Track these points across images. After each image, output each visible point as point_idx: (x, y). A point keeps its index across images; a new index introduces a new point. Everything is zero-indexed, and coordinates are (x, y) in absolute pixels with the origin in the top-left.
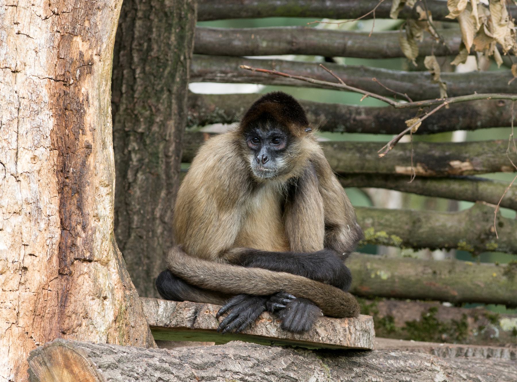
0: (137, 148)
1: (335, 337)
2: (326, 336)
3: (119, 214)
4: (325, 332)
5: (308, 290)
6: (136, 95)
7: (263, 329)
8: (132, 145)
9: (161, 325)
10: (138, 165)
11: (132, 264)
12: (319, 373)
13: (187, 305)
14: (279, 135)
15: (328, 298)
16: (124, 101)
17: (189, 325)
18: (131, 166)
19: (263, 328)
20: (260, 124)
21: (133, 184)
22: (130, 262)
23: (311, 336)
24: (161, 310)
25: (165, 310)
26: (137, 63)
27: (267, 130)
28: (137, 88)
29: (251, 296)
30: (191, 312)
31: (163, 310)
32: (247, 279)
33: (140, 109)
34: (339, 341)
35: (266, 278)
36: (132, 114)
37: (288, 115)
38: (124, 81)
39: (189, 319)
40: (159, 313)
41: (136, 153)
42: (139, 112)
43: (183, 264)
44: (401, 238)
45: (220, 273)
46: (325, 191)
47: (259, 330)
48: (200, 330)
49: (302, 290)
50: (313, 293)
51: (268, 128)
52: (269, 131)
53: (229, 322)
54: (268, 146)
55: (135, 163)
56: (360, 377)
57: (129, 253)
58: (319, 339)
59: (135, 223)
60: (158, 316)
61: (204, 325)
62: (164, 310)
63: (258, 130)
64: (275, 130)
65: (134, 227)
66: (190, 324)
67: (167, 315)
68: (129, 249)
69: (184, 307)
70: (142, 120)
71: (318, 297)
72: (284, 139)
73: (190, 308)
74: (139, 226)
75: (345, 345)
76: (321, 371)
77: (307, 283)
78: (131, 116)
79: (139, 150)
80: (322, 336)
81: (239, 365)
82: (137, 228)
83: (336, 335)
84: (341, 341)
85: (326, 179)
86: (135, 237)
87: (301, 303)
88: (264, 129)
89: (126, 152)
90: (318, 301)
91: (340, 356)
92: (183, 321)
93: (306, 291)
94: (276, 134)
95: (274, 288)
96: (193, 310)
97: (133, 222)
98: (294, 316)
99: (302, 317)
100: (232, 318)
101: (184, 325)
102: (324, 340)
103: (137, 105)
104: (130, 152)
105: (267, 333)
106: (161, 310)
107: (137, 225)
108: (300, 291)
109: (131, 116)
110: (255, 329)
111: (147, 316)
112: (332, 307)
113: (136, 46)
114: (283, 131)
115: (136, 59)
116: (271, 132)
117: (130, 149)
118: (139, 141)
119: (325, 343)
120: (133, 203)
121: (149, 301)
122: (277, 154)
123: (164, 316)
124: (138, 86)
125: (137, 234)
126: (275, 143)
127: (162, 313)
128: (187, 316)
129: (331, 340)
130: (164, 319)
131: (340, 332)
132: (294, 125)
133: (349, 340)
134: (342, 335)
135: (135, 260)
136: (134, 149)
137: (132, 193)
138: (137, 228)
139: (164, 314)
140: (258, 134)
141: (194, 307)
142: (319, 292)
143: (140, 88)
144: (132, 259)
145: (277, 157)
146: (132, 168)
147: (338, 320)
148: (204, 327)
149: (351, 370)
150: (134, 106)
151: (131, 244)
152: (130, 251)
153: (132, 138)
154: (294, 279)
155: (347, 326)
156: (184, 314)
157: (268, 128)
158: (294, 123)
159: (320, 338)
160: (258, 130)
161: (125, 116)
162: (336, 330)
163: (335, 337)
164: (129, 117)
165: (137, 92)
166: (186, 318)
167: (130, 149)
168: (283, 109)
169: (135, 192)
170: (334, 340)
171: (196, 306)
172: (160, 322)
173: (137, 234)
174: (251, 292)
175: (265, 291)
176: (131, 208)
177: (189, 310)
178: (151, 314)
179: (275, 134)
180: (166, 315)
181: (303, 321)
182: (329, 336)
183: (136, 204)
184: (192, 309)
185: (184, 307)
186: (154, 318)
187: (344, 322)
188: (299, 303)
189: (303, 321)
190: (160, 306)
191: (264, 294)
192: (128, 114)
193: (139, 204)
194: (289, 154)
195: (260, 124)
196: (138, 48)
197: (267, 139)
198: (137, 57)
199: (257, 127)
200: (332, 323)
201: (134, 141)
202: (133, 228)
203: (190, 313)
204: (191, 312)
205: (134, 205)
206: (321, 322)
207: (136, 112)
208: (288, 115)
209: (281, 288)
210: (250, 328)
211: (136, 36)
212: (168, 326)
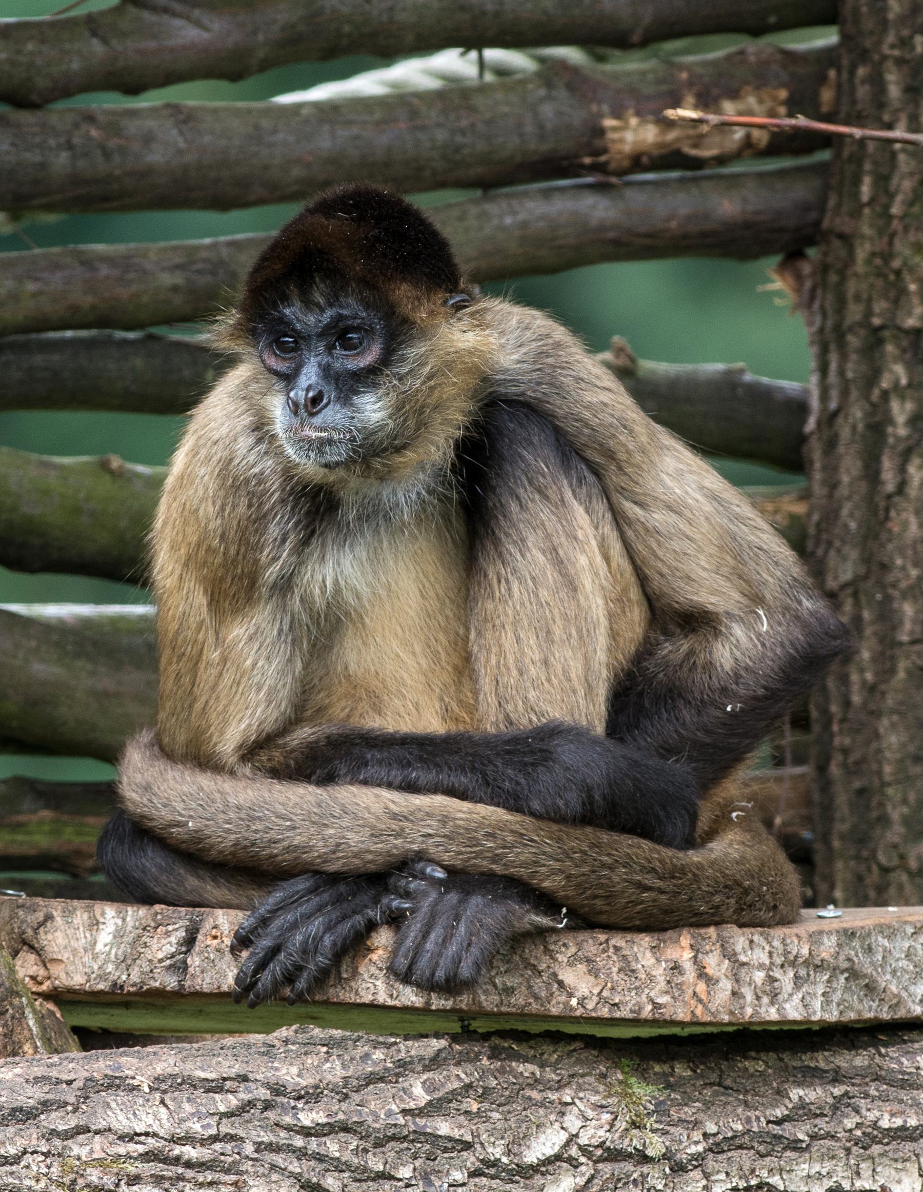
0: (904, 381)
1: (633, 993)
2: (596, 991)
3: (863, 599)
4: (592, 979)
5: (504, 847)
6: (895, 210)
7: (378, 983)
8: (891, 372)
9: (101, 986)
10: (908, 438)
11: (901, 761)
12: (590, 1113)
13: (159, 917)
14: (359, 321)
15: (585, 869)
16: (866, 230)
17: (171, 982)
18: (891, 440)
19: (377, 979)
20: (293, 291)
21: (896, 499)
22: (898, 756)
23: (537, 998)
24: (105, 937)
25: (119, 935)
26: (896, 104)
27: (318, 305)
28: (899, 186)
29: (336, 878)
30: (173, 939)
31: (111, 936)
32: (314, 823)
33: (907, 252)
34: (649, 1007)
35: (367, 815)
36: (886, 271)
37: (385, 255)
38: (868, 166)
39: (168, 962)
40: (99, 947)
41: (903, 398)
42: (905, 264)
46: (637, 510)
47: (364, 985)
48: (199, 995)
49: (481, 852)
50: (526, 855)
51: (321, 301)
52: (322, 310)
53: (262, 966)
55: (902, 432)
56: (823, 1115)
57: (893, 725)
58: (566, 1004)
59: (908, 626)
60: (95, 957)
61: (208, 980)
62: (115, 937)
63: (287, 311)
64: (342, 307)
65: (905, 638)
66: (175, 978)
67: (120, 953)
68: (893, 711)
69: (153, 924)
70: (913, 287)
71: (543, 869)
73: (170, 928)
74: (918, 636)
75: (682, 1015)
76: (602, 1107)
77: (502, 826)
78: (885, 277)
79: (910, 385)
80: (579, 994)
82: (914, 642)
83: (636, 988)
84: (656, 1006)
85: (629, 470)
86: (909, 673)
87: (446, 892)
88: (308, 304)
89: (876, 394)
90: (546, 884)
91: (827, 1047)
92: (151, 971)
93: (499, 851)
94: (346, 317)
95: (395, 847)
96: (182, 934)
97: (901, 622)
98: (425, 935)
99: (445, 941)
100: (266, 954)
101: (157, 984)
102: (590, 1006)
103: (897, 241)
104: (885, 395)
105: (391, 996)
106: (105, 937)
107: (912, 632)
108: (478, 855)
109: (885, 277)
110: (353, 984)
111: (64, 959)
112: (610, 897)
113: (893, 47)
114: (367, 306)
115: (894, 92)
116: (329, 314)
117: (885, 385)
118: (908, 356)
119: (594, 1014)
120: (899, 562)
121: (72, 912)
123: (112, 956)
124: (902, 178)
125: (914, 663)
126: (346, 350)
127: (107, 948)
128: (160, 955)
129: (615, 1005)
130: (110, 968)
131: (651, 978)
132: (404, 287)
133: (700, 1001)
134: (662, 984)
135: (911, 749)
136: (896, 385)
137: (896, 529)
138: (914, 642)
139: (113, 952)
140: (288, 324)
141: (181, 923)
142: (544, 853)
143: (907, 185)
144: (903, 745)
145: (357, 393)
146: (893, 447)
147: (646, 940)
148: (206, 988)
149: (781, 1093)
150: (891, 243)
151: (900, 697)
152: (895, 718)
153: (890, 348)
154: (460, 815)
155: (688, 955)
156: (155, 947)
157: (321, 301)
158: (404, 280)
159: (574, 1002)
160: (287, 311)
161: (872, 279)
162: (633, 971)
163: (633, 993)
164: (879, 283)
165: (899, 198)
166: (161, 961)
167: (885, 385)
168: (366, 238)
169: (905, 525)
170: (630, 1005)
171: (191, 920)
172: (100, 976)
173: (914, 663)
174: (332, 868)
175: (370, 857)
176: (890, 578)
177: (168, 934)
178: (74, 951)
179: (341, 317)
180: (116, 955)
181: (452, 949)
182: (605, 994)
183: (909, 566)
184: (176, 930)
185: (153, 924)
186: (84, 966)
187: (678, 941)
188: (440, 893)
189: (452, 949)
190: (101, 927)
191: (372, 867)
192: (880, 274)
193: (916, 565)
195: (293, 291)
196: (896, 53)
197: (321, 335)
198: (897, 83)
199: (285, 299)
200: (617, 949)
201: (896, 360)
202: (901, 644)
203: (170, 943)
204: (173, 939)
205: (903, 568)
206: (573, 950)
207: (896, 264)
208: (385, 255)
209: (415, 847)
210: (340, 981)
211: (891, 16)
212: (122, 987)
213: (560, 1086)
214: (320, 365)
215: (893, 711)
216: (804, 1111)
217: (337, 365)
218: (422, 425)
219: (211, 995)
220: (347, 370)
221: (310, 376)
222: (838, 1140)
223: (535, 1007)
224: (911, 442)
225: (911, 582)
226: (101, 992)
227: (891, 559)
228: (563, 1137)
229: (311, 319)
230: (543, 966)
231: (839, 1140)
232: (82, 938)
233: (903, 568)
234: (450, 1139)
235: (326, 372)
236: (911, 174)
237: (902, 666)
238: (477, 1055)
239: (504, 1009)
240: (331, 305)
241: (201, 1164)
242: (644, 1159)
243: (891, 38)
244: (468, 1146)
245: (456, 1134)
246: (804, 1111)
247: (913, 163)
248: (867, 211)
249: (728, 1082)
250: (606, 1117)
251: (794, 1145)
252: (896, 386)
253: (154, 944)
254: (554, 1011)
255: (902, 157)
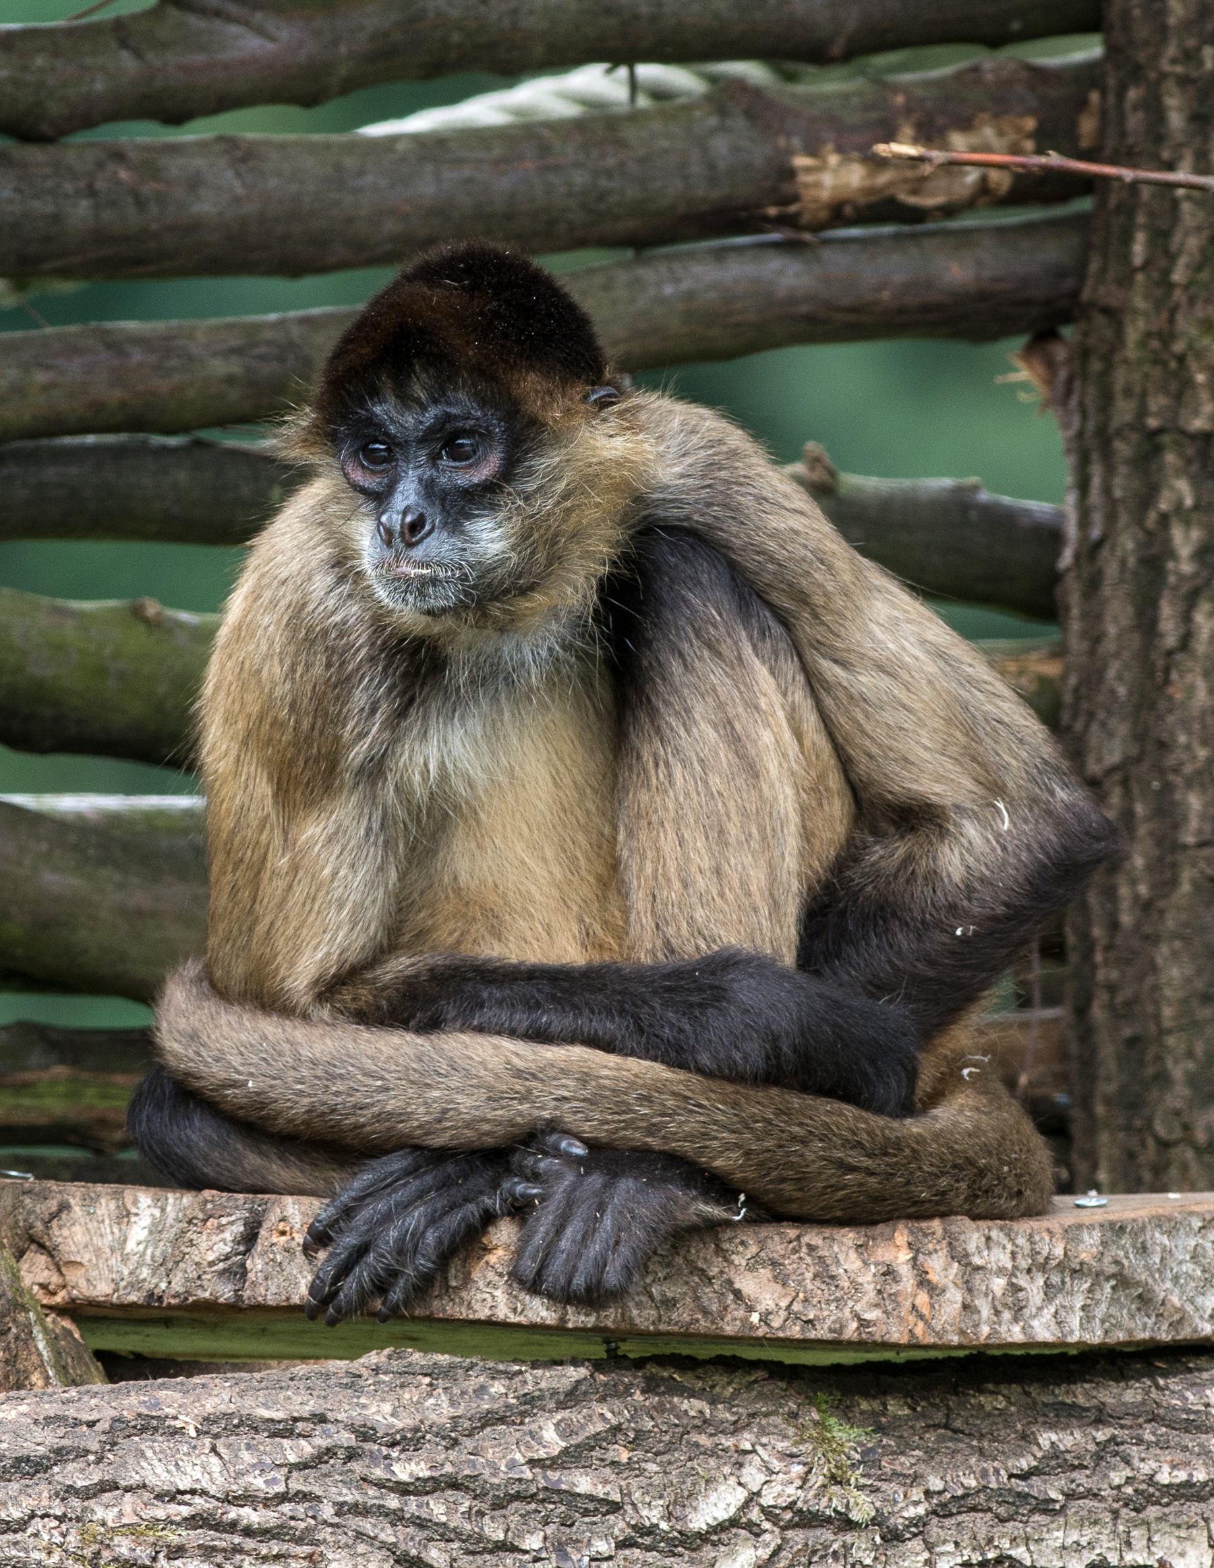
0: (1189, 502)
1: (833, 1307)
2: (784, 1304)
3: (1135, 788)
4: (778, 1287)
5: (663, 1115)
6: (1178, 276)
7: (498, 1293)
8: (1172, 489)
9: (133, 1298)
10: (1195, 576)
11: (1185, 1001)
12: (776, 1465)
13: (209, 1206)
14: (472, 422)
15: (770, 1143)
16: (1139, 303)
17: (225, 1292)
18: (1172, 579)
19: (495, 1287)
20: (386, 382)
21: (1179, 657)
22: (1181, 994)
23: (706, 1312)
24: (138, 1232)
25: (156, 1229)
26: (1179, 137)
27: (418, 401)
28: (1182, 244)
29: (441, 1155)
30: (228, 1236)
31: (146, 1232)
32: (413, 1082)
33: (1193, 332)
34: (854, 1325)
35: (482, 1073)
36: (1166, 356)
37: (506, 336)
38: (1141, 219)
39: (221, 1266)
40: (131, 1246)
41: (1187, 523)
42: (1190, 347)
43: (194, 1036)
44: (1060, 836)
45: (314, 1063)
46: (838, 670)
47: (479, 1296)
48: (261, 1309)
49: (633, 1120)
50: (692, 1124)
51: (423, 395)
52: (424, 408)
53: (344, 1270)
54: (428, 473)
55: (1187, 568)
56: (1082, 1467)
57: (1175, 954)
58: (745, 1321)
59: (1194, 823)
60: (125, 1259)
61: (273, 1289)
62: (151, 1232)
63: (378, 409)
64: (449, 404)
65: (1190, 839)
66: (230, 1287)
67: (157, 1253)
68: (1175, 936)
69: (201, 1216)
70: (1200, 378)
71: (714, 1144)
72: (492, 439)
73: (224, 1221)
74: (1207, 837)
75: (897, 1335)
76: (792, 1456)
77: (660, 1087)
78: (1164, 364)
79: (1196, 507)
80: (761, 1308)
81: (214, 1460)
82: (1202, 845)
83: (837, 1300)
84: (863, 1323)
85: (827, 618)
86: (1196, 885)
87: (587, 1173)
88: (406, 400)
89: (1152, 518)
90: (718, 1163)
91: (1087, 1377)
92: (199, 1278)
93: (657, 1120)
94: (456, 417)
95: (520, 1114)
96: (239, 1228)
97: (1185, 819)
98: (559, 1230)
99: (586, 1238)
100: (350, 1255)
101: (207, 1295)
102: (776, 1323)
103: (1180, 318)
104: (1164, 519)
105: (515, 1310)
106: (138, 1232)
107: (1199, 832)
108: (628, 1124)
109: (1164, 364)
110: (464, 1294)
111: (84, 1261)
112: (802, 1180)
113: (1174, 61)
114: (483, 403)
115: (1176, 120)
116: (432, 413)
117: (1164, 506)
118: (1194, 468)
119: (781, 1334)
120: (1182, 739)
121: (95, 1200)
122: (471, 501)
123: (148, 1258)
124: (1187, 234)
125: (1202, 872)
126: (455, 460)
127: (141, 1247)
128: (211, 1257)
129: (809, 1322)
130: (145, 1273)
131: (856, 1286)
132: (532, 377)
133: (921, 1317)
134: (871, 1295)
135: (1199, 985)
136: (1179, 507)
137: (1178, 696)
138: (1202, 845)
139: (149, 1252)
140: (379, 426)
141: (238, 1214)
142: (716, 1122)
143: (1193, 243)
144: (1188, 980)
145: (469, 517)
146: (1175, 588)
147: (849, 1236)
148: (271, 1300)
149: (1027, 1438)
150: (1171, 320)
151: (1183, 916)
152: (1177, 944)
153: (1170, 458)
154: (605, 1072)
155: (904, 1256)
156: (204, 1246)
157: (423, 395)
158: (531, 368)
159: (755, 1318)
160: (378, 409)
161: (1146, 368)
162: (833, 1277)
163: (833, 1307)
164: (1157, 372)
165: (1183, 261)
166: (211, 1264)
167: (1164, 506)
168: (482, 313)
169: (1191, 690)
170: (828, 1322)
171: (251, 1210)
172: (131, 1284)
173: (1202, 872)
174: (437, 1141)
175: (486, 1127)
176: (1171, 760)
177: (221, 1228)
178: (98, 1252)
179: (448, 418)
180: (153, 1256)
181: (595, 1248)
182: (796, 1307)
183: (1196, 745)
184: (232, 1223)
185: (201, 1216)
186: (111, 1271)
187: (891, 1238)
188: (579, 1175)
189: (595, 1248)
190: (133, 1219)
191: (489, 1141)
192: (1157, 361)
193: (1204, 743)
194: (520, 503)
195: (386, 382)
196: (1179, 69)
197: (422, 441)
198: (1180, 110)
199: (375, 393)
200: (811, 1248)
201: (1178, 473)
202: (1185, 847)
203: (224, 1241)
204: (228, 1236)
205: (1188, 747)
206: (753, 1249)
207: (1179, 347)
208: (506, 336)
209: (546, 1114)
210: (447, 1291)
211: (1172, 21)
212: (160, 1299)
213: (736, 1428)
214: (420, 480)
215: (1175, 936)
216: (1057, 1462)
217: (443, 480)
218: (555, 559)
219: (277, 1309)
220: (456, 487)
221: (407, 494)
222: (1103, 1500)
223: (703, 1325)
224: (1199, 581)
225: (1198, 765)
226: (133, 1305)
227: (1173, 735)
228: (741, 1495)
229: (409, 420)
230: (714, 1271)
231: (1103, 1499)
232: (108, 1234)
233: (1188, 747)
234: (591, 1498)
235: (429, 489)
236: (1199, 229)
237: (1187, 876)
238: (628, 1387)
239: (663, 1327)
240: (435, 401)
241: (265, 1532)
242: (846, 1524)
243: (1172, 50)
244: (615, 1508)
245: (600, 1492)
246: (1057, 1462)
247: (1201, 214)
248: (1140, 277)
249: (958, 1424)
250: (798, 1469)
251: (1045, 1507)
252: (1179, 507)
253: (203, 1241)
254: (729, 1329)
255: (1186, 207)
